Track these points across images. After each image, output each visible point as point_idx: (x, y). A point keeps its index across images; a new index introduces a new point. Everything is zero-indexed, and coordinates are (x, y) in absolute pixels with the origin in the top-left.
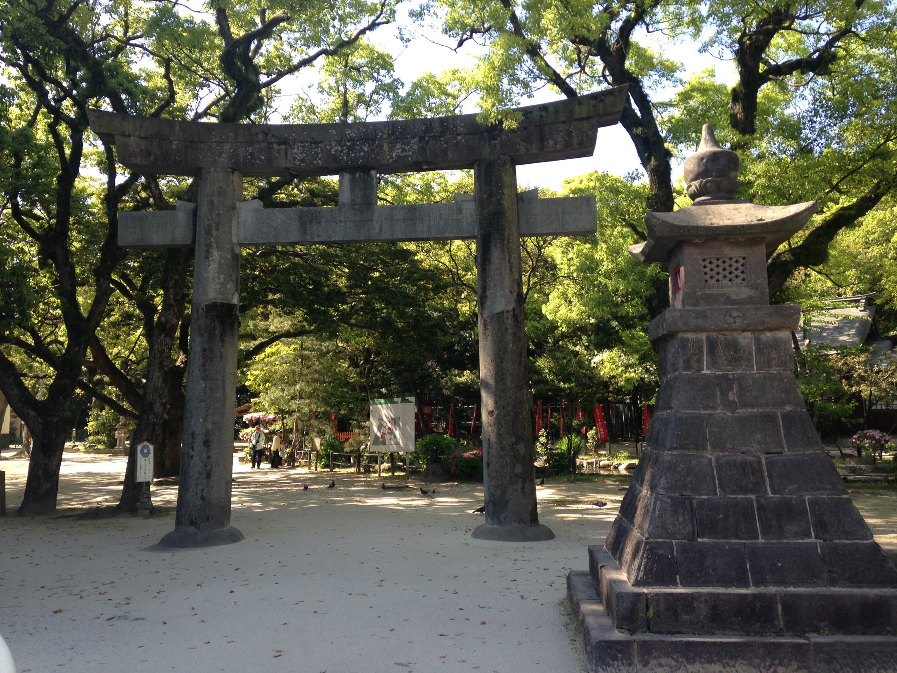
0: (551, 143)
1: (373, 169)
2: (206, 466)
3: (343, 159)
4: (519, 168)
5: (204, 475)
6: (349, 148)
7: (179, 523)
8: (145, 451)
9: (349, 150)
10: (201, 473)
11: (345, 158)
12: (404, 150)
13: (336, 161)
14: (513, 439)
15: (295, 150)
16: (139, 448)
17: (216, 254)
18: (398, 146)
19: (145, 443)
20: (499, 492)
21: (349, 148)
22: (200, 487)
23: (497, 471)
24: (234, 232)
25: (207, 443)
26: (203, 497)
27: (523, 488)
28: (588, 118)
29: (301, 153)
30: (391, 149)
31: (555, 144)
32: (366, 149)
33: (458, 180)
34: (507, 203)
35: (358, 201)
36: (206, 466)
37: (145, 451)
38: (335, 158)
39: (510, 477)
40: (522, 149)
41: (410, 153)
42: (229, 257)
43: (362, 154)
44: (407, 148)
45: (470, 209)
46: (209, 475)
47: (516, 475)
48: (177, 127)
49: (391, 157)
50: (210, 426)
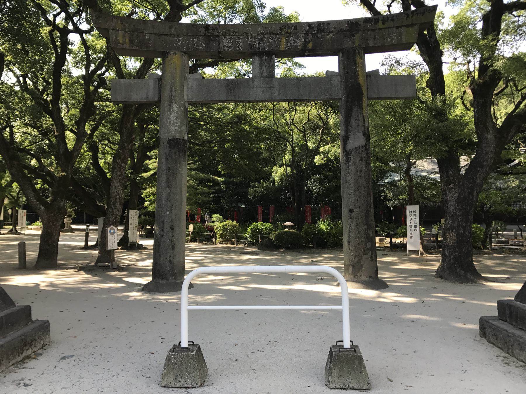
0: (389, 40)
1: (274, 54)
2: (172, 242)
3: (255, 47)
4: (367, 56)
5: (170, 247)
6: (260, 40)
7: (154, 277)
8: (112, 231)
9: (260, 41)
10: (169, 246)
11: (257, 46)
12: (295, 42)
13: (251, 48)
14: (366, 227)
15: (224, 41)
16: (109, 229)
17: (175, 107)
18: (291, 39)
19: (112, 226)
20: (356, 260)
21: (260, 40)
22: (169, 255)
23: (355, 247)
24: (185, 93)
25: (172, 228)
26: (170, 261)
27: (371, 257)
28: (422, 102)
29: (228, 42)
30: (287, 41)
31: (392, 40)
32: (271, 41)
33: (329, 64)
34: (361, 80)
35: (265, 74)
36: (172, 242)
37: (112, 231)
38: (251, 46)
39: (364, 251)
40: (371, 44)
41: (299, 44)
42: (182, 109)
43: (268, 44)
44: (297, 41)
45: (337, 81)
46: (173, 247)
47: (368, 249)
48: (149, 25)
49: (287, 46)
50: (173, 217)
